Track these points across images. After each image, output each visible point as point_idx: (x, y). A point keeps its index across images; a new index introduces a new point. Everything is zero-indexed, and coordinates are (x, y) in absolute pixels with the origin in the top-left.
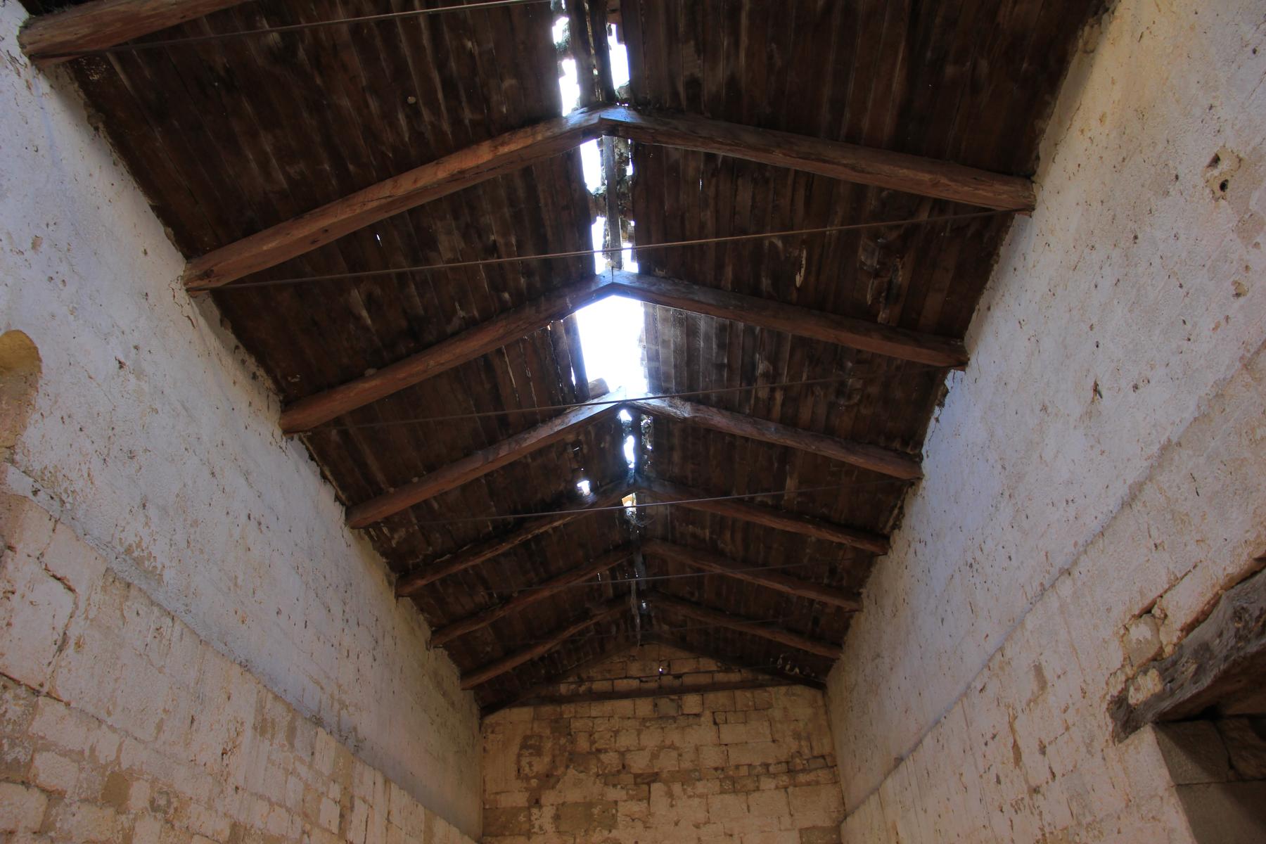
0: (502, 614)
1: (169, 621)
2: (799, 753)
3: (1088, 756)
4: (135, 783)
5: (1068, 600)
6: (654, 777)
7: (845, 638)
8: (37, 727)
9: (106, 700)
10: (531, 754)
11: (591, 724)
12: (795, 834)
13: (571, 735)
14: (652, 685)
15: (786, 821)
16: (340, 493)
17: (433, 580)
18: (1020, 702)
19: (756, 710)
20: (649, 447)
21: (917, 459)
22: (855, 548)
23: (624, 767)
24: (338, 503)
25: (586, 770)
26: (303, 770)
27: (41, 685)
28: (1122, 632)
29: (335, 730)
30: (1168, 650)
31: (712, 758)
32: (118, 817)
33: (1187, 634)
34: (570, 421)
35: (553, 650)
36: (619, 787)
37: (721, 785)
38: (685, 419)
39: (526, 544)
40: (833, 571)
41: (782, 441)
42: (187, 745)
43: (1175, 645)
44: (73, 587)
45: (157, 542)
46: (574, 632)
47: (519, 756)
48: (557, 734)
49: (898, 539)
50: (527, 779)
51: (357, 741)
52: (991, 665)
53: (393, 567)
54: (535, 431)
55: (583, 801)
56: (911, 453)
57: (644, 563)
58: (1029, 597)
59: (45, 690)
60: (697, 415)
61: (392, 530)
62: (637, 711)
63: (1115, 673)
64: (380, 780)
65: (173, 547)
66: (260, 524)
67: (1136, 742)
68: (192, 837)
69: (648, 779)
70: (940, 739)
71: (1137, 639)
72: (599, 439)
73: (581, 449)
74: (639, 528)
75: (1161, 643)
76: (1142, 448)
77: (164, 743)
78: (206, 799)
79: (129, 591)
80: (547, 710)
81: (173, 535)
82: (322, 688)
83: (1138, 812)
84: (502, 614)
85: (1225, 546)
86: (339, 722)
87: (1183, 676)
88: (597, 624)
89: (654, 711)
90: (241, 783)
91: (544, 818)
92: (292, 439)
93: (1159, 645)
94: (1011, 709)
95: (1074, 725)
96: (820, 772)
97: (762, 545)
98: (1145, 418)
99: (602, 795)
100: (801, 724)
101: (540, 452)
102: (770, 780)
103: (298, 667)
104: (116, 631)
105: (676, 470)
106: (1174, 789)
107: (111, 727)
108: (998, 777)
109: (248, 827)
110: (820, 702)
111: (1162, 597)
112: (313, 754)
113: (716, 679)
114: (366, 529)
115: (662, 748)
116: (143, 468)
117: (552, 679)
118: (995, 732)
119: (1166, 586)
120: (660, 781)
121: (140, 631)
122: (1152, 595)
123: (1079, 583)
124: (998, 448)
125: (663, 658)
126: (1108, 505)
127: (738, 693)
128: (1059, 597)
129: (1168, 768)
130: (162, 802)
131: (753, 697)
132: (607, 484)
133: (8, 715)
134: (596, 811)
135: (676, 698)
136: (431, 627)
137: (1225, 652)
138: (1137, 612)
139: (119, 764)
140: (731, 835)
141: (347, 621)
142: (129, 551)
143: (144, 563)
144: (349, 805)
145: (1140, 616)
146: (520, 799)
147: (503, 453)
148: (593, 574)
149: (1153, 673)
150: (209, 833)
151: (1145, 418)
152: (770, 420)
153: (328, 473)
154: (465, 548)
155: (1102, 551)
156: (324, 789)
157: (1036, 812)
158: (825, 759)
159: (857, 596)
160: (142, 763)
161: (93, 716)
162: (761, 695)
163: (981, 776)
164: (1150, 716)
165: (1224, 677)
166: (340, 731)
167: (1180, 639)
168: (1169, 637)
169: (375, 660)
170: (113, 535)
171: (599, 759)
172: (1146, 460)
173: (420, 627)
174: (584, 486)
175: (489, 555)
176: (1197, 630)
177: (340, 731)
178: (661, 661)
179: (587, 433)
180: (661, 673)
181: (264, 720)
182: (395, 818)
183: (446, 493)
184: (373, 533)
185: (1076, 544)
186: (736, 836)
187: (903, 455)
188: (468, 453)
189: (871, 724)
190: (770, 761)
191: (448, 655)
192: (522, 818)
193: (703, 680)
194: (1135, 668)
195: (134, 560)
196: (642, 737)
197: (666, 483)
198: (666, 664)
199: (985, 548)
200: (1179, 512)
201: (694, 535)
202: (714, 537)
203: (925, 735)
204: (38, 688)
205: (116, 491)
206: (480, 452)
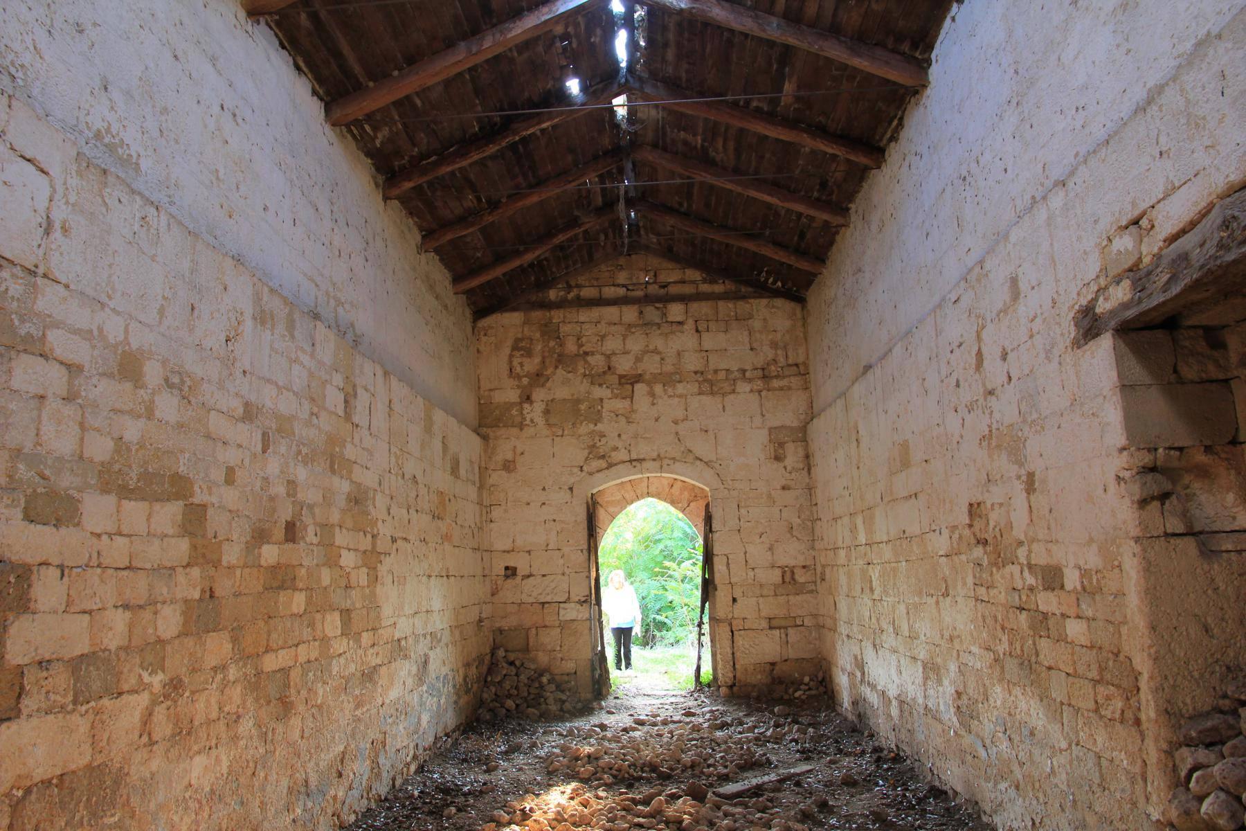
0: (491, 219)
1: (153, 211)
2: (775, 361)
3: (1046, 361)
4: (147, 363)
5: (1057, 212)
6: (638, 378)
7: (830, 253)
8: (41, 305)
9: (104, 284)
10: (522, 355)
11: (579, 329)
12: (766, 432)
13: (560, 339)
14: (640, 293)
15: (758, 420)
16: (317, 87)
17: (419, 182)
18: (991, 312)
19: (736, 320)
20: (642, 43)
21: (925, 65)
22: (848, 160)
23: (609, 368)
24: (315, 98)
25: (574, 371)
26: (305, 359)
27: (36, 266)
28: (1105, 243)
29: (333, 325)
30: (1146, 260)
31: (692, 362)
32: (137, 391)
33: (1169, 245)
34: (557, 10)
35: (542, 257)
36: (605, 386)
37: (700, 387)
38: (682, 10)
39: (513, 147)
40: (823, 185)
41: (784, 38)
42: (191, 330)
43: (1154, 256)
44: (45, 170)
45: (128, 129)
46: (562, 239)
47: (511, 356)
48: (546, 337)
49: (894, 153)
50: (519, 377)
51: (355, 336)
52: (968, 277)
53: (379, 167)
54: (520, 20)
55: (570, 398)
56: (920, 57)
57: (634, 169)
58: (1018, 210)
59: (41, 271)
60: (695, 6)
61: (376, 129)
62: (623, 318)
63: (1089, 284)
64: (380, 373)
65: (146, 135)
66: (234, 115)
67: (1094, 348)
68: (209, 412)
69: (631, 380)
70: (909, 348)
71: (1118, 251)
72: (590, 32)
73: (570, 43)
74: (629, 133)
75: (1141, 253)
76: (1174, 45)
77: (168, 328)
78: (217, 380)
79: (106, 178)
80: (537, 315)
81: (143, 122)
82: (317, 285)
83: (1080, 410)
84: (491, 219)
85: (1235, 151)
86: (336, 317)
87: (1155, 285)
88: (586, 232)
89: (640, 319)
90: (248, 368)
91: (535, 412)
92: (258, 24)
93: (1139, 256)
94: (980, 319)
95: (1038, 333)
96: (793, 379)
97: (754, 154)
98: (1188, 8)
99: (589, 393)
100: (779, 336)
101: (527, 45)
102: (746, 384)
103: (291, 263)
104: (101, 217)
105: (670, 70)
106: (1118, 389)
107: (114, 310)
108: (958, 381)
109: (260, 406)
110: (799, 315)
111: (1153, 207)
112: (313, 345)
113: (700, 289)
114: (348, 126)
115: (646, 352)
116: (96, 46)
117: (543, 285)
118: (961, 340)
119: (1161, 196)
120: (642, 382)
121: (125, 219)
122: (1144, 206)
123: (1071, 195)
124: (1015, 49)
125: (650, 268)
126: (1120, 112)
127: (721, 303)
128: (1049, 209)
129: (1118, 371)
130: (176, 380)
131: (736, 308)
132: (598, 84)
133: (10, 293)
134: (583, 407)
135: (662, 306)
136: (421, 232)
137: (1202, 261)
138: (1124, 223)
139: (129, 344)
140: (706, 431)
141: (336, 221)
142: (98, 136)
143: (117, 150)
144: (352, 393)
145: (1126, 227)
146: (512, 395)
147: (487, 43)
148: (582, 181)
149: (1126, 283)
150: (225, 410)
151: (1188, 8)
152: (773, 14)
153: (302, 64)
154: (451, 150)
155: (1104, 160)
156: (328, 377)
157: (987, 412)
158: (798, 367)
159: (844, 212)
160: (151, 344)
161: (94, 299)
162: (743, 307)
163: (942, 381)
164: (1113, 324)
165: (1196, 285)
166: (338, 326)
167: (1161, 249)
168: (1151, 247)
169: (367, 261)
170: (78, 118)
171: (586, 362)
172: (1175, 58)
173: (410, 230)
174: (573, 86)
175: (476, 158)
176: (1180, 240)
177: (338, 326)
178: (647, 271)
179: (577, 25)
180: (647, 282)
181: (263, 311)
182: (397, 406)
183: (428, 88)
184: (355, 132)
185: (1077, 155)
186: (710, 433)
187: (910, 59)
188: (450, 45)
189: (846, 335)
190: (747, 367)
191: (440, 260)
192: (514, 412)
193: (688, 290)
194: (1109, 279)
195: (106, 146)
196: (627, 342)
197: (659, 84)
198: (652, 273)
199: (982, 160)
200: (1196, 116)
201: (686, 143)
202: (706, 144)
203: (895, 344)
204: (33, 269)
205: (71, 68)
206: (462, 44)
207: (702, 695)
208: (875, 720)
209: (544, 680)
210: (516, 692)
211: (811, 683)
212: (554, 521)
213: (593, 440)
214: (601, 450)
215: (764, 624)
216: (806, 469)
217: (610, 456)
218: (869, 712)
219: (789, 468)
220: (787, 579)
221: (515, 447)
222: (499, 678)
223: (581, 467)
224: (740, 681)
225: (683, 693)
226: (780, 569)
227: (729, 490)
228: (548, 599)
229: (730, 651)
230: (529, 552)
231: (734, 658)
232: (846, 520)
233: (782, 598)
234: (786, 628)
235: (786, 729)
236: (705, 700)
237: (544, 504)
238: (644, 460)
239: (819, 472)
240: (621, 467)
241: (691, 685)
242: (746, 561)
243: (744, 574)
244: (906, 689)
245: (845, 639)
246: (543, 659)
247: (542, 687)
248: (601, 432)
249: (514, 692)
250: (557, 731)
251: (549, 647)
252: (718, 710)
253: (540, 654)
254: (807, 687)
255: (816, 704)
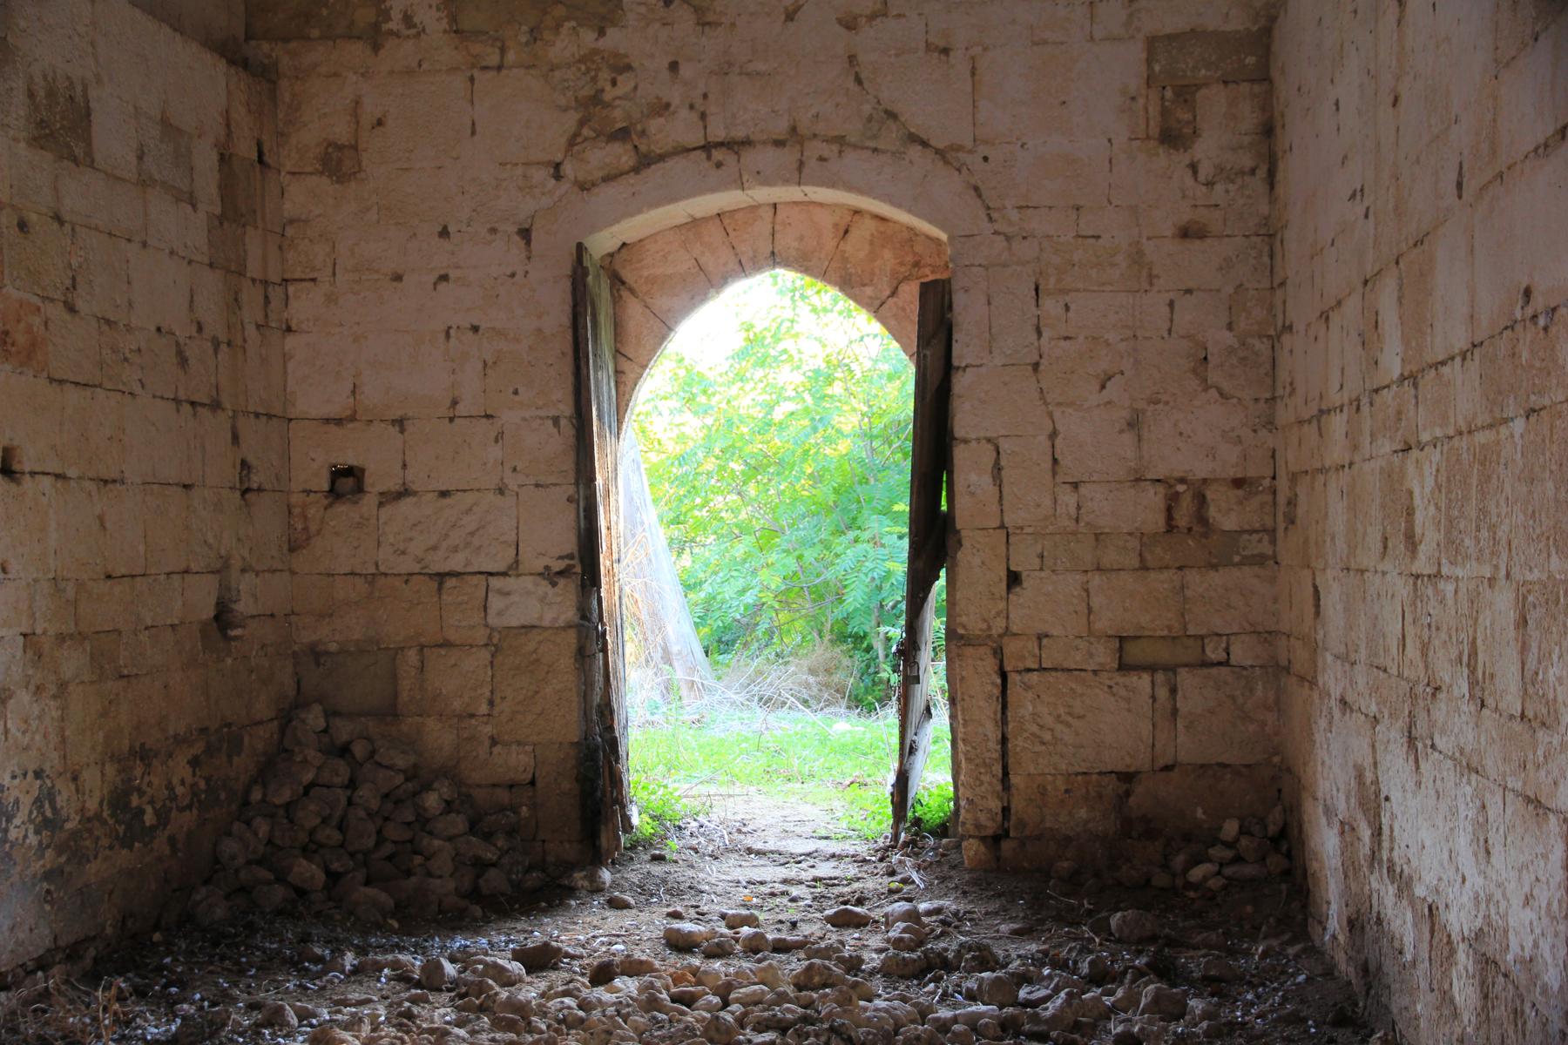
12: (1135, 52)
186: (957, 57)
207: (909, 862)
208: (1405, 1001)
209: (432, 801)
210: (337, 836)
211: (1244, 842)
212: (475, 329)
213: (594, 80)
214: (617, 113)
215: (1104, 655)
216: (1262, 172)
217: (643, 133)
218: (1389, 967)
219: (1205, 171)
220: (1183, 517)
221: (357, 102)
222: (286, 795)
223: (557, 166)
224: (1022, 824)
225: (862, 849)
226: (1161, 489)
227: (1008, 238)
228: (456, 563)
229: (993, 733)
230: (400, 423)
231: (1004, 755)
232: (1352, 306)
233: (1165, 575)
234: (1171, 669)
235: (1120, 993)
236: (915, 876)
237: (444, 278)
238: (747, 143)
239: (1292, 170)
240: (675, 165)
241: (881, 821)
242: (1055, 461)
243: (1048, 502)
244: (1504, 917)
245: (1337, 713)
246: (439, 738)
247: (423, 821)
248: (616, 55)
249: (330, 835)
250: (395, 965)
251: (457, 705)
252: (938, 911)
253: (432, 724)
254: (1229, 854)
255: (1249, 909)
